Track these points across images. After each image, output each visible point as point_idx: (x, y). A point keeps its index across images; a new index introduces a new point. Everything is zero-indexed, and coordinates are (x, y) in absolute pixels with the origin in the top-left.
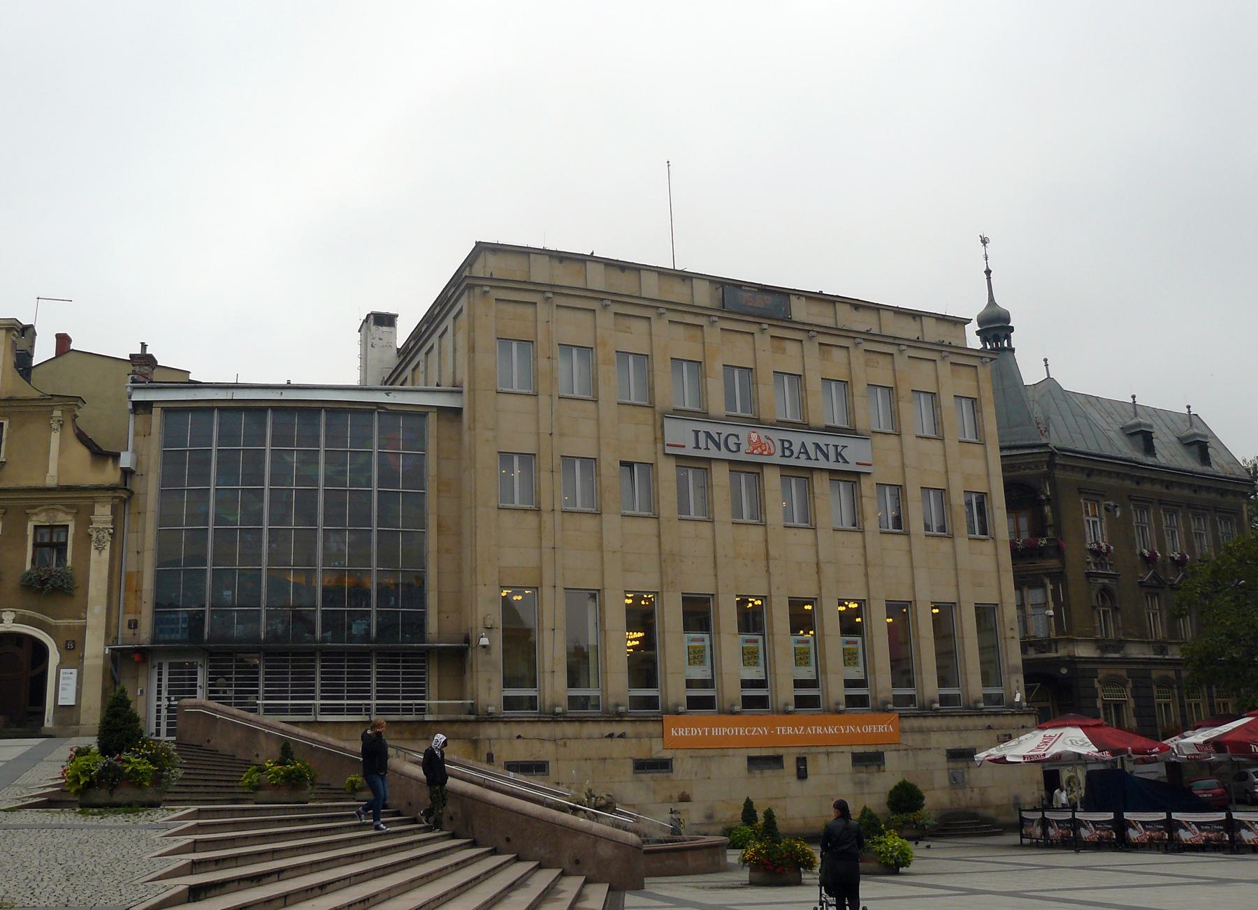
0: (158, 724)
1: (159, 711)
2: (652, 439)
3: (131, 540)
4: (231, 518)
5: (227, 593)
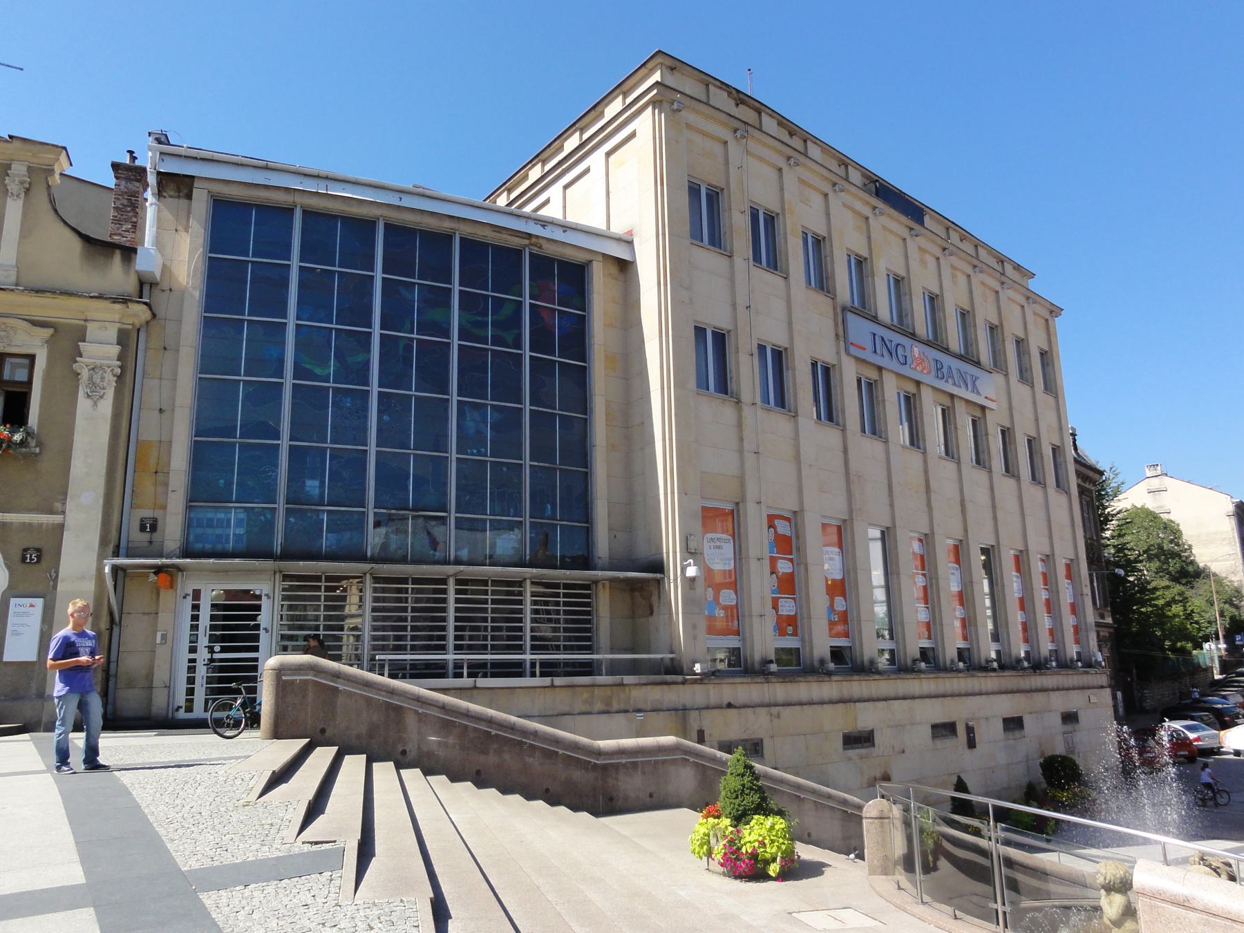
0: (190, 692)
1: (192, 669)
2: (833, 335)
3: (151, 392)
4: (318, 371)
5: (312, 485)
